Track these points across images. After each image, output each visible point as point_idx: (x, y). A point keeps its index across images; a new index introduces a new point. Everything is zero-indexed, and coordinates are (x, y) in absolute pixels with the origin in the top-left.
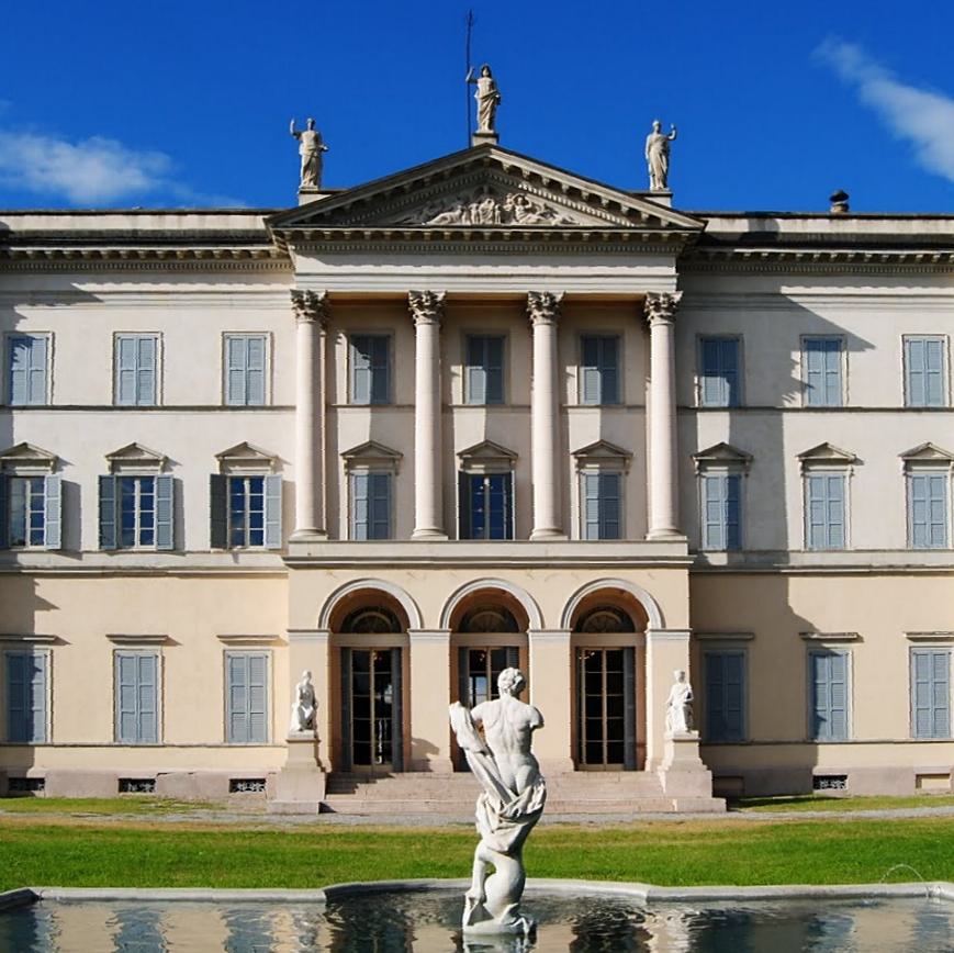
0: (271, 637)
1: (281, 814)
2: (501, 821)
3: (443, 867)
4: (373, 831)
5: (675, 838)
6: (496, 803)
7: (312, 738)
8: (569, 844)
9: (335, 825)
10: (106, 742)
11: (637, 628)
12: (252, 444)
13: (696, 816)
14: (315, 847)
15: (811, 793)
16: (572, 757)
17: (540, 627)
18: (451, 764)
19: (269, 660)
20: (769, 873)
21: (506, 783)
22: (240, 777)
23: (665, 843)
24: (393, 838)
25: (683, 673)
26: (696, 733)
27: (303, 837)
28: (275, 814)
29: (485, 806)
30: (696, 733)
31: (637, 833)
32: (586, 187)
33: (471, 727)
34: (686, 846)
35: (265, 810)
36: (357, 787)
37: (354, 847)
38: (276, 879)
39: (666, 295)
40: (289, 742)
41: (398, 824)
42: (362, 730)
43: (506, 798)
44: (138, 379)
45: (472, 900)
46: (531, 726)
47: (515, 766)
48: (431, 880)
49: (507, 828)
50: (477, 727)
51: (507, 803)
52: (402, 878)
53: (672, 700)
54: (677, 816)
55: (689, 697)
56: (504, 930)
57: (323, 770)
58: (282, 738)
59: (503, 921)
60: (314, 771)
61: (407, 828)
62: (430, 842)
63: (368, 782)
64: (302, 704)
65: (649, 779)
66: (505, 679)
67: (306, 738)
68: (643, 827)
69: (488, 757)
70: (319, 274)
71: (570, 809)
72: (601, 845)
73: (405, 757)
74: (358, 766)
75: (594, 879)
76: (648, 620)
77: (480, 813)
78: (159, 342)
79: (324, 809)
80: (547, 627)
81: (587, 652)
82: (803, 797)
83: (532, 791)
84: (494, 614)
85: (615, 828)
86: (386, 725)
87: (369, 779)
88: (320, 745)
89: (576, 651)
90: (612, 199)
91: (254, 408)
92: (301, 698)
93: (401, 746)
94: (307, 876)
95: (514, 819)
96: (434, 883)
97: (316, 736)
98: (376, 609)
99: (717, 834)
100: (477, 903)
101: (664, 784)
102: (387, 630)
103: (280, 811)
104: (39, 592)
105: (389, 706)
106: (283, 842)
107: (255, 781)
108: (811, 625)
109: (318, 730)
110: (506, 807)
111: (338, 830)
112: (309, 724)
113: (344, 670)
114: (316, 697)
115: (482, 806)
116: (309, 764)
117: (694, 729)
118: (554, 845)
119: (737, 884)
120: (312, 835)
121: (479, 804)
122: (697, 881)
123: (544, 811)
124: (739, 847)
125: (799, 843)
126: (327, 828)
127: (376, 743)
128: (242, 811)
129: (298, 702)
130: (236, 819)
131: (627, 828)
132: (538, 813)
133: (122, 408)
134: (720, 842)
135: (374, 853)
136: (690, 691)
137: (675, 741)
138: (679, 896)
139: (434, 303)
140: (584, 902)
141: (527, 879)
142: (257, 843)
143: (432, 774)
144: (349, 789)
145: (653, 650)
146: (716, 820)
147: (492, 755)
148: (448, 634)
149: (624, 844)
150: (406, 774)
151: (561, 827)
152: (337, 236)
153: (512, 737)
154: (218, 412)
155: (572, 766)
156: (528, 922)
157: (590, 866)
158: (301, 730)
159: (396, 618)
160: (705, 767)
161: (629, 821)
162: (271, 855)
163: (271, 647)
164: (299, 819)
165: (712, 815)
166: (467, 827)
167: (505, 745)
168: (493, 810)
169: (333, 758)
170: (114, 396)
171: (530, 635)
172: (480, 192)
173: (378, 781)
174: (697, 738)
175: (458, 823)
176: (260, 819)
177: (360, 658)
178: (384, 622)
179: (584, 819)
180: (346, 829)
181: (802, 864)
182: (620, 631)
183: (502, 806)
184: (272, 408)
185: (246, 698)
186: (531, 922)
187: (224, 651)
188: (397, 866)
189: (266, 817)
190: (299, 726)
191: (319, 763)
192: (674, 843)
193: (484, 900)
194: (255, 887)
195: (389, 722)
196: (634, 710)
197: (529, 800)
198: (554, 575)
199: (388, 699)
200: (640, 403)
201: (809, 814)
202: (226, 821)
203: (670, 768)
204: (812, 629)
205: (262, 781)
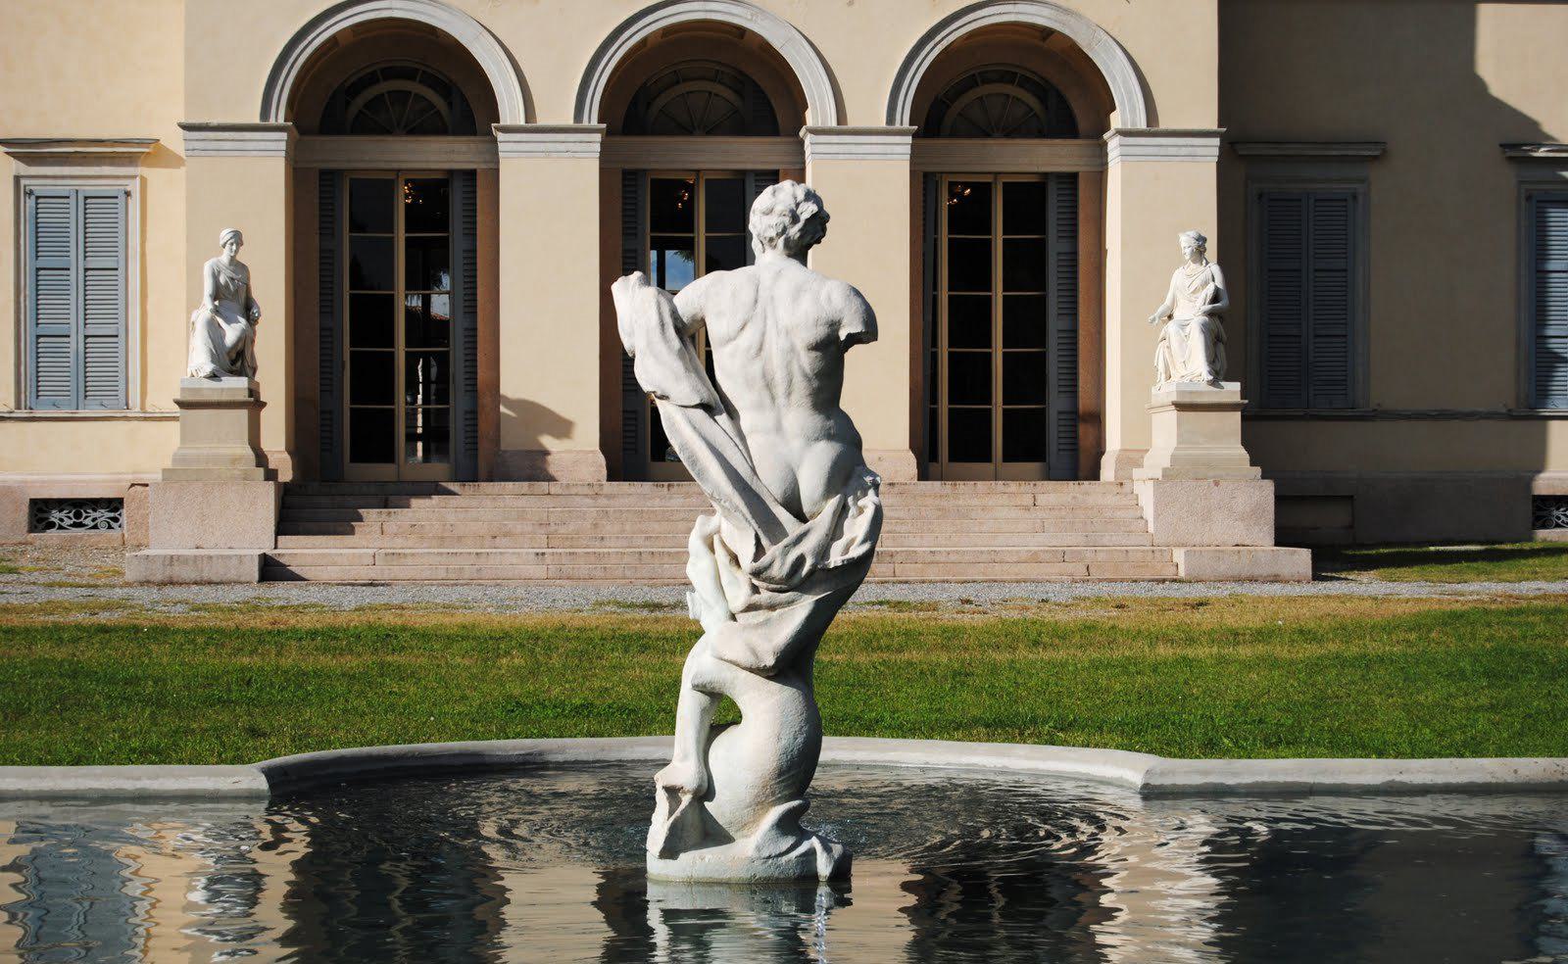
0: (141, 143)
1: (162, 584)
2: (755, 590)
3: (584, 710)
4: (399, 622)
5: (1191, 641)
6: (742, 538)
7: (244, 396)
8: (915, 656)
9: (305, 607)
11: (1083, 124)
13: (1238, 589)
14: (246, 660)
15: (1531, 539)
16: (914, 446)
17: (832, 123)
18: (601, 459)
19: (134, 204)
20: (1462, 727)
21: (771, 487)
22: (56, 495)
23: (1164, 651)
24: (466, 636)
25: (1201, 240)
26: (1236, 386)
27: (215, 637)
28: (145, 583)
29: (712, 549)
30: (1236, 386)
31: (1090, 627)
33: (676, 343)
34: (1221, 661)
35: (120, 574)
36: (360, 519)
37: (351, 663)
38: (135, 743)
40: (182, 404)
41: (466, 606)
42: (373, 379)
43: (769, 526)
45: (673, 792)
46: (843, 335)
47: (796, 443)
48: (495, 742)
49: (772, 607)
50: (692, 336)
51: (774, 541)
52: (475, 738)
53: (1172, 308)
54: (1186, 588)
55: (1215, 299)
56: (761, 870)
57: (271, 475)
58: (163, 400)
59: (758, 849)
60: (246, 477)
61: (485, 612)
62: (549, 649)
63: (386, 505)
64: (216, 311)
65: (1111, 500)
66: (769, 212)
67: (225, 398)
68: (1101, 615)
69: (723, 419)
71: (910, 572)
72: (1002, 657)
73: (484, 447)
74: (362, 467)
75: (990, 738)
76: (1113, 108)
77: (698, 567)
79: (271, 570)
80: (853, 122)
81: (952, 185)
82: (1508, 547)
83: (842, 512)
84: (718, 88)
85: (1029, 615)
86: (434, 371)
87: (392, 496)
88: (264, 413)
89: (925, 185)
92: (215, 296)
93: (473, 414)
94: (219, 732)
95: (795, 582)
96: (562, 750)
97: (253, 392)
98: (409, 74)
99: (1301, 632)
100: (686, 799)
101: (1149, 513)
102: (440, 129)
103: (159, 577)
105: (443, 324)
106: (160, 652)
107: (95, 503)
108: (1533, 125)
109: (257, 378)
110: (772, 551)
111: (307, 622)
112: (236, 360)
113: (328, 228)
114: (255, 294)
115: (703, 550)
116: (235, 460)
117: (1229, 379)
118: (875, 657)
119: (1381, 754)
120: (239, 633)
121: (695, 542)
122: (1271, 746)
123: (877, 569)
124: (1366, 663)
125: (1525, 656)
126: (276, 614)
127: (409, 408)
128: (58, 577)
129: (207, 305)
130: (43, 596)
131: (1063, 617)
132: (857, 569)
134: (1310, 651)
135: (401, 674)
136: (1219, 282)
137: (1181, 407)
138: (1231, 781)
140: (933, 796)
141: (824, 738)
142: (89, 654)
143: (554, 488)
144: (339, 522)
145: (1125, 183)
146: (1290, 600)
147: (733, 414)
148: (598, 137)
149: (1061, 655)
150: (486, 487)
151: (889, 614)
153: (788, 365)
155: (914, 470)
156: (828, 849)
157: (975, 707)
158: (214, 376)
159: (464, 99)
160: (1257, 470)
161: (1062, 599)
162: (127, 682)
163: (140, 170)
164: (207, 595)
165: (1277, 587)
166: (645, 613)
167: (769, 386)
168: (735, 560)
169: (298, 445)
171: (808, 139)
173: (415, 502)
174: (1237, 398)
175: (618, 604)
176: (105, 595)
177: (373, 193)
178: (432, 106)
179: (944, 596)
180: (329, 619)
181: (1545, 706)
182: (1042, 133)
183: (760, 550)
185: (74, 299)
186: (837, 849)
187: (17, 179)
188: (462, 708)
189: (119, 592)
190: (209, 367)
191: (261, 459)
192: (1190, 652)
193: (705, 792)
194: (77, 761)
195: (443, 360)
196: (1074, 331)
197: (835, 531)
199: (440, 306)
201: (1528, 588)
202: (15, 601)
203: (1166, 474)
204: (1540, 137)
205: (114, 504)
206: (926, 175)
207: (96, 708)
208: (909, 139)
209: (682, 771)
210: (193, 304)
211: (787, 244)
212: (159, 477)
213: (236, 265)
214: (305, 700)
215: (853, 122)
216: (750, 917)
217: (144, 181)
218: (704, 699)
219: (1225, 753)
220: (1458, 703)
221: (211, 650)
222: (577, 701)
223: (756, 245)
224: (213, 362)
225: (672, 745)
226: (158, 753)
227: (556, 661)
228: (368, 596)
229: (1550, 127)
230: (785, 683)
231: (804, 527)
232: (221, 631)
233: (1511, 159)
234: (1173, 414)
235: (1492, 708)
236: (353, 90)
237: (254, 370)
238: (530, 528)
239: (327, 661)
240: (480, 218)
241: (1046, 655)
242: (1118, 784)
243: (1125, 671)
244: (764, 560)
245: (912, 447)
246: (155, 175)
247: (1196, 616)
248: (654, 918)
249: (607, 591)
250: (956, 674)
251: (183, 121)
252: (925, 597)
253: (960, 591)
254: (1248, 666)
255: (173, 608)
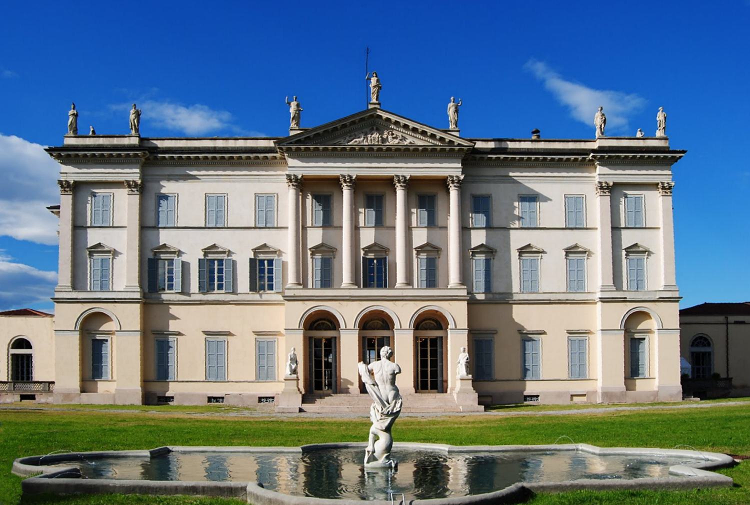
1: (282, 413)
2: (382, 416)
3: (355, 437)
4: (323, 420)
5: (461, 424)
6: (379, 407)
8: (413, 426)
10: (202, 380)
11: (444, 327)
12: (268, 244)
13: (471, 413)
14: (297, 428)
17: (399, 328)
18: (359, 390)
19: (276, 343)
21: (384, 399)
22: (263, 396)
23: (456, 426)
24: (335, 423)
25: (465, 349)
26: (471, 376)
27: (291, 423)
28: (279, 412)
29: (374, 409)
30: (471, 376)
31: (444, 421)
32: (421, 127)
34: (466, 427)
36: (316, 401)
37: (315, 428)
39: (457, 176)
40: (285, 380)
42: (318, 375)
43: (384, 405)
44: (217, 215)
45: (368, 452)
46: (396, 372)
47: (388, 391)
50: (371, 373)
51: (384, 408)
54: (462, 414)
55: (467, 359)
56: (383, 466)
57: (301, 393)
58: (282, 378)
59: (383, 461)
61: (339, 419)
62: (349, 425)
63: (321, 398)
65: (449, 397)
66: (383, 351)
67: (293, 378)
69: (376, 387)
70: (299, 167)
71: (413, 411)
72: (427, 427)
73: (338, 387)
74: (316, 391)
77: (372, 412)
78: (226, 198)
79: (301, 410)
80: (403, 328)
83: (396, 402)
85: (434, 419)
88: (299, 381)
89: (416, 338)
90: (432, 132)
91: (269, 228)
92: (291, 360)
93: (336, 382)
95: (388, 415)
96: (351, 444)
97: (297, 377)
98: (325, 320)
100: (371, 453)
101: (456, 399)
102: (330, 329)
104: (171, 312)
105: (331, 363)
106: (282, 426)
107: (270, 398)
108: (523, 327)
110: (384, 409)
111: (307, 420)
112: (294, 372)
113: (310, 347)
116: (294, 390)
117: (470, 374)
118: (406, 427)
120: (296, 422)
121: (372, 408)
123: (401, 411)
125: (518, 426)
126: (302, 419)
127: (325, 380)
128: (263, 411)
129: (289, 362)
130: (261, 415)
132: (398, 412)
133: (209, 228)
134: (482, 425)
135: (324, 430)
136: (468, 356)
137: (461, 379)
138: (463, 450)
139: (351, 180)
140: (419, 453)
142: (271, 426)
144: (312, 401)
148: (358, 331)
149: (438, 427)
150: (338, 395)
151: (409, 419)
152: (307, 149)
153: (387, 378)
154: (253, 230)
156: (394, 462)
157: (422, 436)
158: (291, 374)
160: (475, 391)
162: (277, 431)
163: (277, 337)
164: (290, 415)
167: (384, 381)
168: (378, 411)
169: (305, 387)
170: (206, 222)
171: (395, 331)
172: (372, 129)
173: (326, 398)
174: (471, 378)
177: (318, 342)
178: (328, 325)
181: (519, 435)
183: (382, 409)
184: (277, 228)
185: (266, 360)
186: (395, 462)
187: (256, 339)
189: (274, 414)
190: (290, 373)
191: (299, 390)
192: (460, 426)
193: (374, 452)
195: (331, 371)
196: (442, 366)
197: (395, 406)
198: (406, 304)
199: (330, 360)
200: (393, 225)
201: (522, 413)
205: (273, 398)
206: (416, 337)
207: (272, 436)
208: (413, 331)
209: (369, 448)
210: (287, 361)
211: (386, 357)
212: (281, 393)
213: (294, 354)
214: (308, 435)
215: (403, 328)
216: (381, 474)
217: (278, 339)
218: (374, 435)
219: (464, 445)
220: (504, 435)
221: (291, 426)
222: (354, 435)
223: (381, 357)
224: (290, 371)
225: (368, 443)
226: (283, 444)
227: (350, 427)
228: (318, 415)
229: (525, 327)
230: (387, 433)
231: (389, 406)
232: (293, 422)
233: (520, 333)
234: (460, 381)
235: (510, 436)
236: (314, 323)
237: (297, 373)
238: (321, 432)
239: (311, 428)
240: (337, 345)
241: (435, 427)
242: (444, 450)
243: (449, 430)
244: (383, 411)
245: (414, 387)
246: (280, 338)
247: (462, 419)
248: (365, 473)
249: (360, 414)
250: (420, 430)
251: (285, 328)
252: (415, 415)
253: (422, 414)
254: (470, 429)
255: (283, 417)
